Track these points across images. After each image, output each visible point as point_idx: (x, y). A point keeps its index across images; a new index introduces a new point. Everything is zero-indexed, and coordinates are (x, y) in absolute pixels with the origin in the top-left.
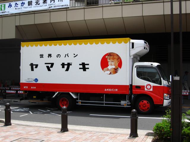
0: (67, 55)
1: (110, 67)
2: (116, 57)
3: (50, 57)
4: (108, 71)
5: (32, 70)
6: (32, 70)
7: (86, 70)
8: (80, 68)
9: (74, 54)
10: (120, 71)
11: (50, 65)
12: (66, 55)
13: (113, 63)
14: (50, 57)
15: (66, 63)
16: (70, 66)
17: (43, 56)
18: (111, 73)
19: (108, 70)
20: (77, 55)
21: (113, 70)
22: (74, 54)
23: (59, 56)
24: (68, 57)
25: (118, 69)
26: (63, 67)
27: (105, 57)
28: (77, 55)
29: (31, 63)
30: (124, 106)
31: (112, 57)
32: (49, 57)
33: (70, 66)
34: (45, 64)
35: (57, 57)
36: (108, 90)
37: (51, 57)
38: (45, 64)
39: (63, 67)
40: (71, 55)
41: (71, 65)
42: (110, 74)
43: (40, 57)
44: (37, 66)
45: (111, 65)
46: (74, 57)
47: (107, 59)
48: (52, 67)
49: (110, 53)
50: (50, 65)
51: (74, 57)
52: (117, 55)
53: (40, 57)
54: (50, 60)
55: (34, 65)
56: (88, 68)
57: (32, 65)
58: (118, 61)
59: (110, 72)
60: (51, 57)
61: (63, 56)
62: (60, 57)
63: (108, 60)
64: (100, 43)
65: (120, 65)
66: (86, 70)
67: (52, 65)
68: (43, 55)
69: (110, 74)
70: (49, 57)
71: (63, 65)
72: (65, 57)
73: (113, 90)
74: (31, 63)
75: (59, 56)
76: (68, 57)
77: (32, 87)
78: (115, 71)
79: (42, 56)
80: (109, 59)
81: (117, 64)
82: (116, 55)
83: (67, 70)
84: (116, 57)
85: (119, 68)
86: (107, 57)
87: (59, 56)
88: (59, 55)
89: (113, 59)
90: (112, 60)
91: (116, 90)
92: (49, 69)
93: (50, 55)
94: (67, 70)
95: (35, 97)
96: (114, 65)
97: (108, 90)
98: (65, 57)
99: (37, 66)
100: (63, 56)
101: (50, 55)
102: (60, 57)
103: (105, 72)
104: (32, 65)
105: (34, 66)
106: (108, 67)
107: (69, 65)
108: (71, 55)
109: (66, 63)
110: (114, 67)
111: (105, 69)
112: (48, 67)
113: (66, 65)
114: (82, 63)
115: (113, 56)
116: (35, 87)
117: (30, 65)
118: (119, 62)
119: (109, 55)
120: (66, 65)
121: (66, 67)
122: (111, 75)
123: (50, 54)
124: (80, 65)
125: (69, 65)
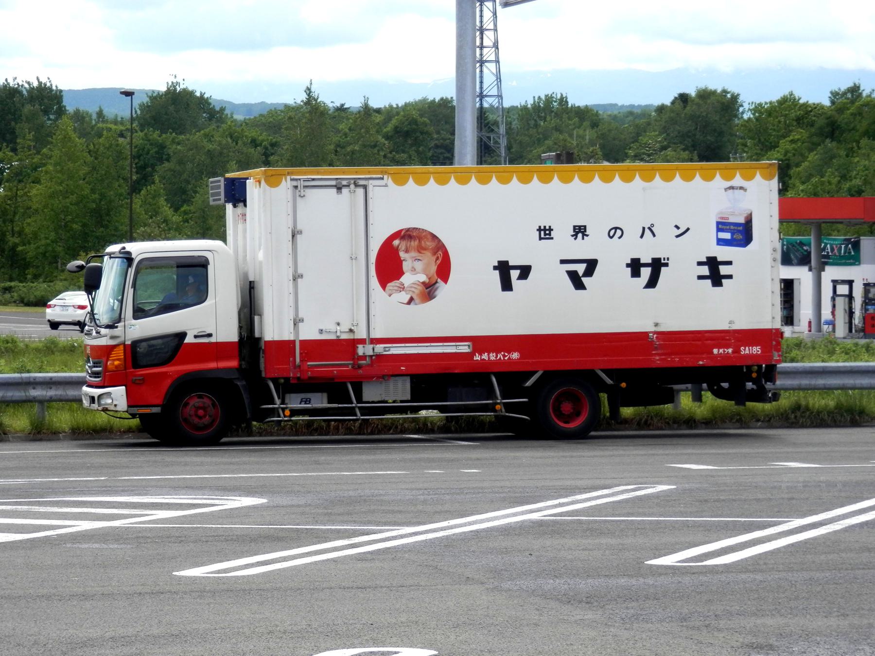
0: (649, 228)
1: (407, 279)
2: (430, 244)
3: (580, 235)
4: (403, 293)
5: (507, 285)
6: (507, 285)
7: (724, 281)
8: (700, 277)
9: (677, 227)
10: (444, 290)
11: (581, 268)
12: (644, 228)
13: (419, 265)
14: (580, 235)
15: (646, 259)
16: (663, 269)
17: (550, 234)
18: (411, 300)
19: (402, 288)
20: (688, 229)
21: (421, 288)
22: (677, 227)
23: (615, 232)
24: (654, 235)
25: (437, 285)
26: (636, 273)
27: (392, 246)
28: (688, 229)
29: (499, 262)
30: (386, 402)
31: (414, 243)
32: (575, 236)
33: (663, 269)
34: (563, 262)
35: (611, 237)
36: (485, 356)
37: (584, 235)
38: (563, 262)
39: (636, 273)
40: (666, 232)
41: (666, 265)
42: (409, 303)
43: (541, 239)
44: (525, 272)
45: (413, 270)
46: (677, 236)
47: (396, 251)
48: (589, 272)
49: (408, 230)
50: (581, 268)
51: (677, 236)
52: (434, 237)
53: (541, 239)
54: (582, 249)
55: (515, 268)
56: (730, 277)
57: (503, 268)
58: (437, 259)
59: (408, 297)
60: (584, 235)
61: (632, 231)
62: (620, 238)
63: (402, 254)
64: (640, 176)
65: (444, 271)
66: (724, 281)
67: (591, 265)
68: (550, 230)
69: (409, 303)
70: (575, 236)
71: (635, 266)
72: (642, 236)
73: (504, 356)
74: (499, 262)
75: (619, 232)
76: (654, 235)
77: (715, 351)
78: (428, 291)
79: (545, 233)
80: (407, 251)
81: (434, 268)
82: (429, 237)
83: (652, 283)
84: (430, 244)
85: (441, 283)
86: (396, 242)
87: (615, 232)
88: (616, 228)
89: (420, 249)
90: (414, 254)
91: (515, 356)
92: (577, 282)
93: (580, 231)
94: (652, 283)
95: (725, 385)
96: (425, 272)
97: (485, 356)
98: (642, 236)
99: (525, 272)
100: (632, 231)
101: (580, 231)
102: (620, 238)
103: (390, 295)
104: (503, 268)
105: (514, 274)
106: (403, 279)
107: (657, 265)
108: (666, 232)
109: (646, 259)
110: (423, 278)
111: (391, 286)
112: (574, 277)
113: (646, 265)
114: (708, 258)
115: (420, 239)
116: (730, 350)
117: (628, 265)
118: (439, 262)
119: (406, 235)
120: (646, 265)
121: (646, 272)
122: (412, 306)
123: (580, 227)
124: (700, 264)
125: (657, 265)
